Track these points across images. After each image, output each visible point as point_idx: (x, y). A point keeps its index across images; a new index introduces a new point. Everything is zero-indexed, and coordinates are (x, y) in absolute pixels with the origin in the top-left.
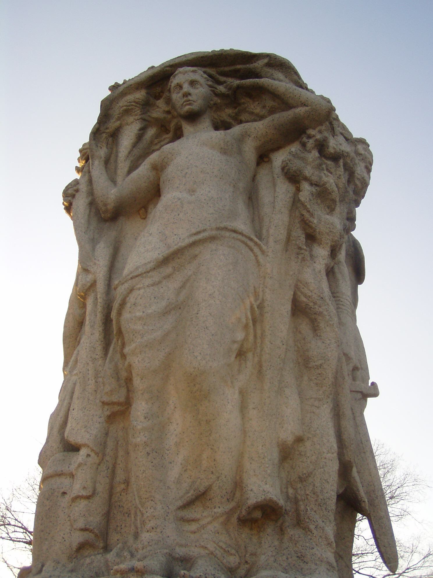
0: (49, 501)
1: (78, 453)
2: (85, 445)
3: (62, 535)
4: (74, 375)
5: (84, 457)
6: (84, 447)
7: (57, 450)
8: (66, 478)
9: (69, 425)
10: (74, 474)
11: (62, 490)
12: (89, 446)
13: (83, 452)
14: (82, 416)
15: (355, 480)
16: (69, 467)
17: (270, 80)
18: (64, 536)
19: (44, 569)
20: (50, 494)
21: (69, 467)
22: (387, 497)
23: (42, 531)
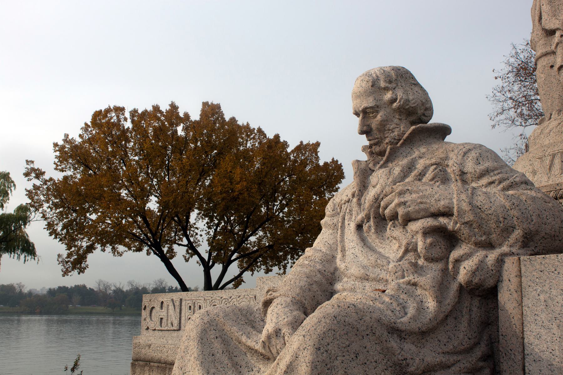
0: (543, 74)
1: (554, 36)
2: (558, 29)
3: (558, 93)
4: (408, 219)
5: (559, 38)
6: (557, 30)
7: (542, 36)
8: (550, 56)
9: (543, 18)
10: (555, 51)
11: (550, 65)
12: (560, 29)
13: (558, 34)
14: (550, 8)
15: (320, 329)
16: (550, 48)
17: (391, 205)
18: (559, 94)
19: (552, 116)
20: (543, 69)
21: (550, 48)
22: (557, 255)
23: (545, 94)
